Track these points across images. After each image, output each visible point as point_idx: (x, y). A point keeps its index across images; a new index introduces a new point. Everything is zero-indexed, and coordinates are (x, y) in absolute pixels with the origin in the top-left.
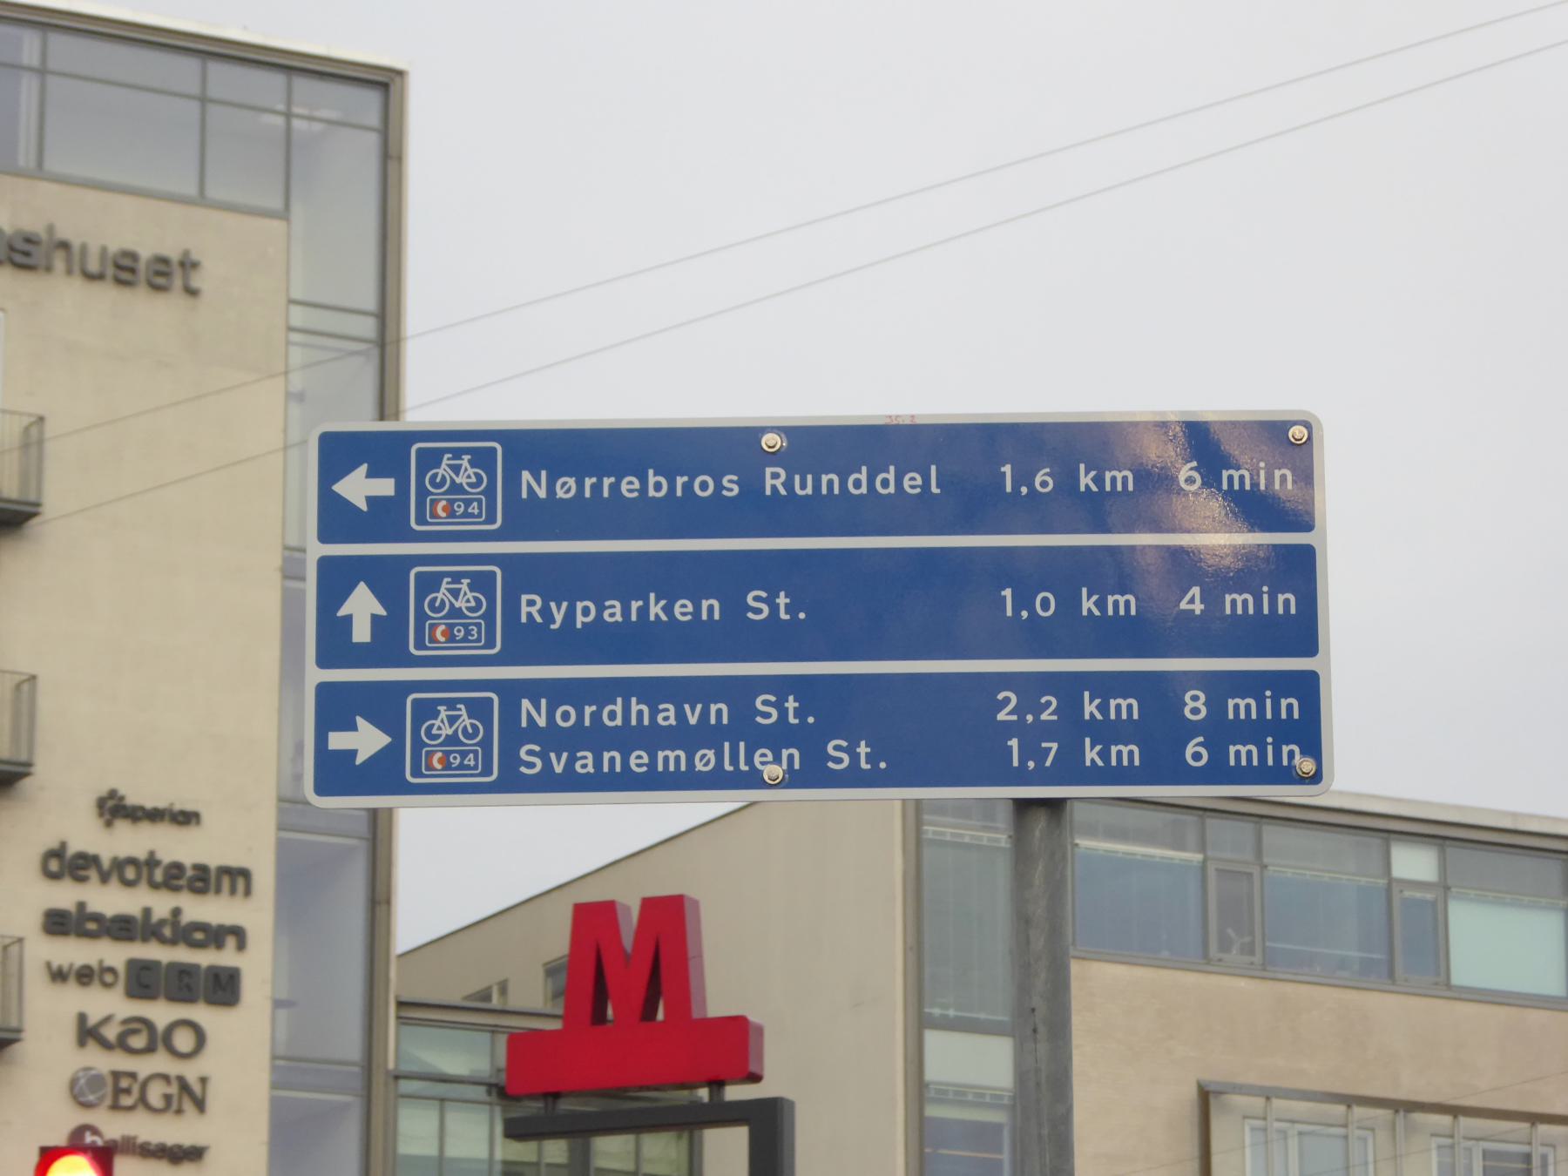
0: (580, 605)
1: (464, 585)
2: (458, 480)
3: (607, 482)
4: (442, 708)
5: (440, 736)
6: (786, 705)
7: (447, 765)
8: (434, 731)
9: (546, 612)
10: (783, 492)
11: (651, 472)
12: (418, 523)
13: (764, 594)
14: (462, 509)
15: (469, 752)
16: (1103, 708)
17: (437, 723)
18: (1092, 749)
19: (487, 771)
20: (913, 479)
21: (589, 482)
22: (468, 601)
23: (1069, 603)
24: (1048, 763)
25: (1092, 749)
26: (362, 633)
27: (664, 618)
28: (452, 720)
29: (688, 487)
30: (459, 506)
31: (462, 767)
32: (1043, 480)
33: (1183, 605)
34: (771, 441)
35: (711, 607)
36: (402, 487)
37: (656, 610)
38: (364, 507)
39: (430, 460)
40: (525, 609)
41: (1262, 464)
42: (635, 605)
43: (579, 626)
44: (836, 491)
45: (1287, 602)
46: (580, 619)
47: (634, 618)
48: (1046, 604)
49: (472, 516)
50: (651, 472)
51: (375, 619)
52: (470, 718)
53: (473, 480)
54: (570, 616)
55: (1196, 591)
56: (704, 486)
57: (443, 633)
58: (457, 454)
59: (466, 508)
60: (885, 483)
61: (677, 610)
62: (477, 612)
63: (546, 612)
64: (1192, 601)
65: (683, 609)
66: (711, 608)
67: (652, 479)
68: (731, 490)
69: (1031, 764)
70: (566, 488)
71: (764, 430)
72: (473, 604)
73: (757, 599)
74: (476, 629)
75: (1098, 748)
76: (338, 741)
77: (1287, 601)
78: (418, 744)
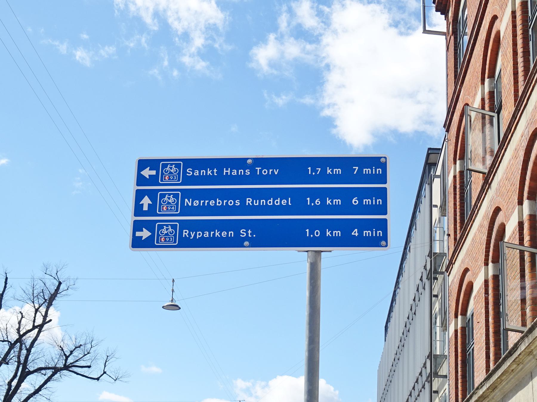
0: (198, 233)
2: (169, 201)
3: (206, 202)
4: (165, 227)
5: (164, 233)
6: (248, 232)
8: (162, 232)
9: (189, 234)
10: (251, 204)
11: (218, 199)
12: (161, 181)
13: (245, 230)
14: (170, 208)
15: (173, 206)
16: (332, 202)
17: (163, 230)
18: (329, 170)
19: (177, 211)
20: (284, 201)
21: (202, 202)
22: (174, 170)
23: (323, 233)
24: (318, 173)
25: (329, 170)
26: (145, 208)
27: (219, 236)
28: (167, 229)
29: (227, 203)
30: (169, 208)
31: (171, 210)
33: (353, 234)
34: (249, 161)
36: (157, 173)
37: (217, 234)
40: (184, 234)
41: (374, 167)
42: (212, 233)
43: (198, 238)
44: (265, 204)
45: (379, 201)
47: (211, 236)
49: (172, 210)
50: (218, 199)
52: (171, 229)
53: (173, 201)
54: (195, 235)
55: (356, 230)
56: (231, 203)
57: (163, 239)
58: (172, 164)
59: (171, 208)
60: (277, 202)
61: (223, 234)
62: (176, 173)
63: (189, 234)
64: (355, 233)
65: (224, 234)
66: (231, 234)
67: (218, 201)
68: (237, 202)
69: (314, 174)
70: (196, 203)
71: (248, 159)
72: (173, 201)
73: (243, 231)
74: (172, 238)
75: (330, 232)
76: (138, 234)
78: (158, 235)
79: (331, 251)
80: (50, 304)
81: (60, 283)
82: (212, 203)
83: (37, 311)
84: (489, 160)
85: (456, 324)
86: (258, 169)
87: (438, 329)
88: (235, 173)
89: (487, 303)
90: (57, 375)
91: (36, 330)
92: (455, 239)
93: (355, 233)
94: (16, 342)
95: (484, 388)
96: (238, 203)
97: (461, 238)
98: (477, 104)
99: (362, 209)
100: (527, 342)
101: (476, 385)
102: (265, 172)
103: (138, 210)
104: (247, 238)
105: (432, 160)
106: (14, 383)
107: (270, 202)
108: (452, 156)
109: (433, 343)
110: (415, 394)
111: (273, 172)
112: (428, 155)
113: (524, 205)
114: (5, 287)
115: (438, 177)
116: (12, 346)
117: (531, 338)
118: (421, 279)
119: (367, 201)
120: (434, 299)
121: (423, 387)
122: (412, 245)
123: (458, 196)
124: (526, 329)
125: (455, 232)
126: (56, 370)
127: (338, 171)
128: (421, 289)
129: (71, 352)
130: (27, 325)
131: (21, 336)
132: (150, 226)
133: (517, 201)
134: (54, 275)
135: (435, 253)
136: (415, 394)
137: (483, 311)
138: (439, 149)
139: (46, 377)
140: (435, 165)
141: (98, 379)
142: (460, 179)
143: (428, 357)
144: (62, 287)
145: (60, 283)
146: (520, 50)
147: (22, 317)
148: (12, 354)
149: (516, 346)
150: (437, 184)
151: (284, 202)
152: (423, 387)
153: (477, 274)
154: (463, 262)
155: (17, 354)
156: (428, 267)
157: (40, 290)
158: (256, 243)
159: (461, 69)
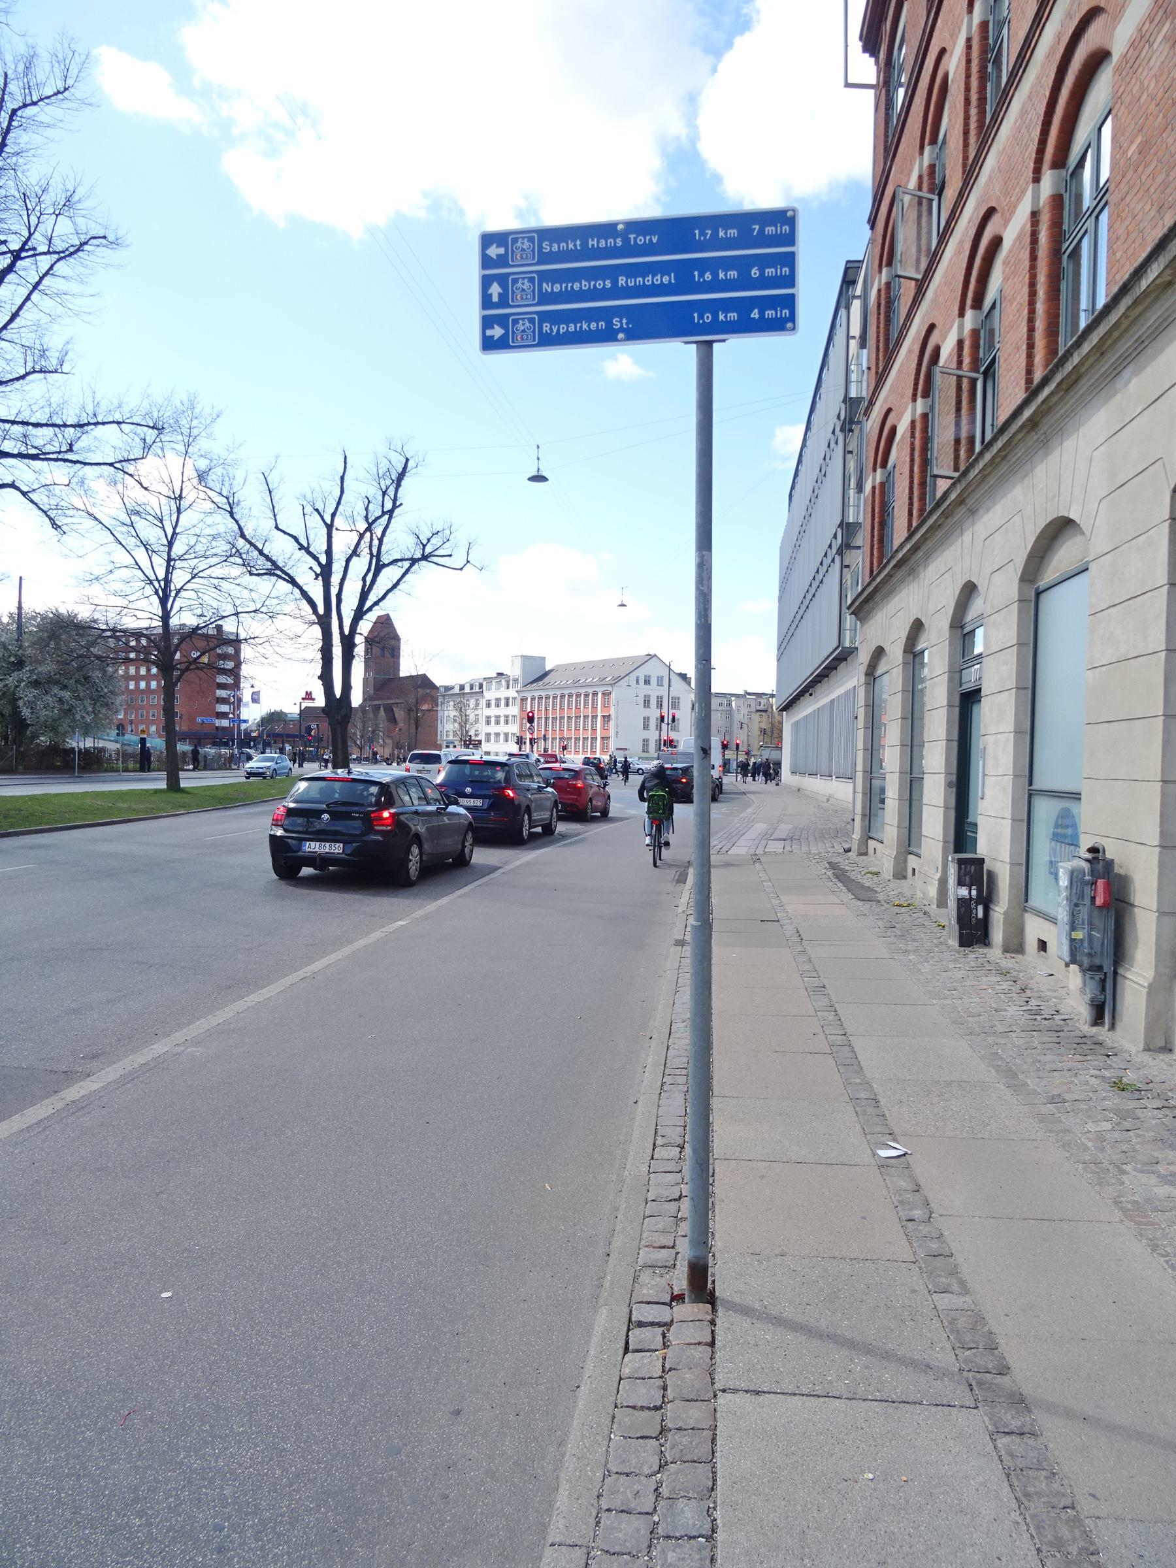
1: (526, 281)
7: (522, 298)
9: (551, 329)
19: (534, 299)
21: (564, 285)
23: (715, 317)
26: (495, 299)
28: (523, 324)
29: (595, 285)
32: (708, 276)
33: (752, 316)
35: (602, 324)
37: (585, 327)
38: (495, 257)
39: (515, 241)
42: (578, 325)
46: (562, 331)
48: (708, 317)
51: (497, 247)
54: (558, 330)
63: (551, 329)
65: (593, 326)
67: (583, 283)
76: (489, 333)
77: (786, 270)
78: (513, 333)
79: (724, 341)
80: (398, 486)
81: (407, 460)
82: (576, 286)
83: (384, 493)
84: (923, 265)
85: (874, 479)
86: (632, 236)
87: (852, 492)
88: (602, 244)
89: (912, 449)
90: (416, 567)
91: (387, 517)
92: (877, 373)
93: (755, 314)
94: (365, 532)
95: (905, 550)
96: (608, 284)
97: (884, 369)
98: (912, 184)
99: (764, 283)
100: (959, 489)
101: (895, 548)
102: (641, 240)
103: (486, 302)
104: (621, 330)
105: (850, 278)
106: (369, 579)
107: (649, 280)
108: (877, 262)
109: (846, 508)
110: (823, 570)
111: (651, 240)
112: (846, 270)
113: (966, 317)
114: (345, 467)
115: (859, 297)
116: (361, 536)
117: (964, 483)
118: (833, 433)
119: (770, 271)
120: (844, 570)
121: (833, 561)
122: (822, 390)
123: (881, 335)
124: (956, 475)
125: (877, 364)
126: (414, 561)
127: (733, 316)
128: (833, 445)
129: (429, 540)
130: (375, 511)
131: (370, 525)
132: (502, 321)
133: (957, 312)
134: (399, 450)
135: (851, 398)
136: (823, 570)
137: (908, 459)
138: (860, 261)
139: (403, 570)
140: (853, 282)
141: (461, 569)
142: (886, 294)
143: (839, 526)
144: (410, 464)
145: (407, 460)
146: (974, 97)
147: (369, 502)
148: (362, 544)
149: (946, 495)
150: (856, 305)
151: (666, 279)
152: (833, 561)
153: (902, 414)
154: (885, 400)
155: (368, 544)
156: (842, 417)
157: (385, 469)
158: (634, 335)
159: (894, 136)
